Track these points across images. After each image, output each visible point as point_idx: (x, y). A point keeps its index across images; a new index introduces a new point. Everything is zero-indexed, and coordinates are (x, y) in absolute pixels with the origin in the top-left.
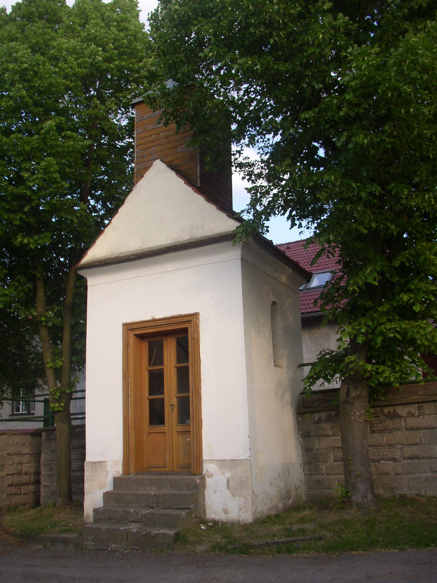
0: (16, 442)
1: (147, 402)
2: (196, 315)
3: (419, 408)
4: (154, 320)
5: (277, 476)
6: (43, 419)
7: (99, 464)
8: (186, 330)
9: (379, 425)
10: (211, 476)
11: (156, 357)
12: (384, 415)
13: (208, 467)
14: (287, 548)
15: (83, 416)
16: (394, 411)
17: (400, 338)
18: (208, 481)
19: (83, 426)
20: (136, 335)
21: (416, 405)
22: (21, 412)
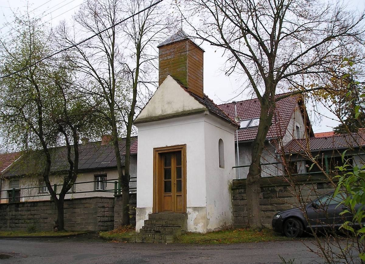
0: (102, 201)
1: (164, 182)
2: (185, 145)
3: (284, 188)
4: (167, 147)
5: (219, 216)
6: (114, 191)
7: (143, 209)
8: (180, 152)
9: (267, 195)
10: (190, 214)
11: (167, 163)
12: (270, 191)
13: (188, 210)
14: (221, 243)
15: (135, 190)
16: (274, 189)
17: (124, 175)
18: (189, 216)
19: (135, 195)
20: (159, 153)
21: (283, 187)
22: (99, 189)
